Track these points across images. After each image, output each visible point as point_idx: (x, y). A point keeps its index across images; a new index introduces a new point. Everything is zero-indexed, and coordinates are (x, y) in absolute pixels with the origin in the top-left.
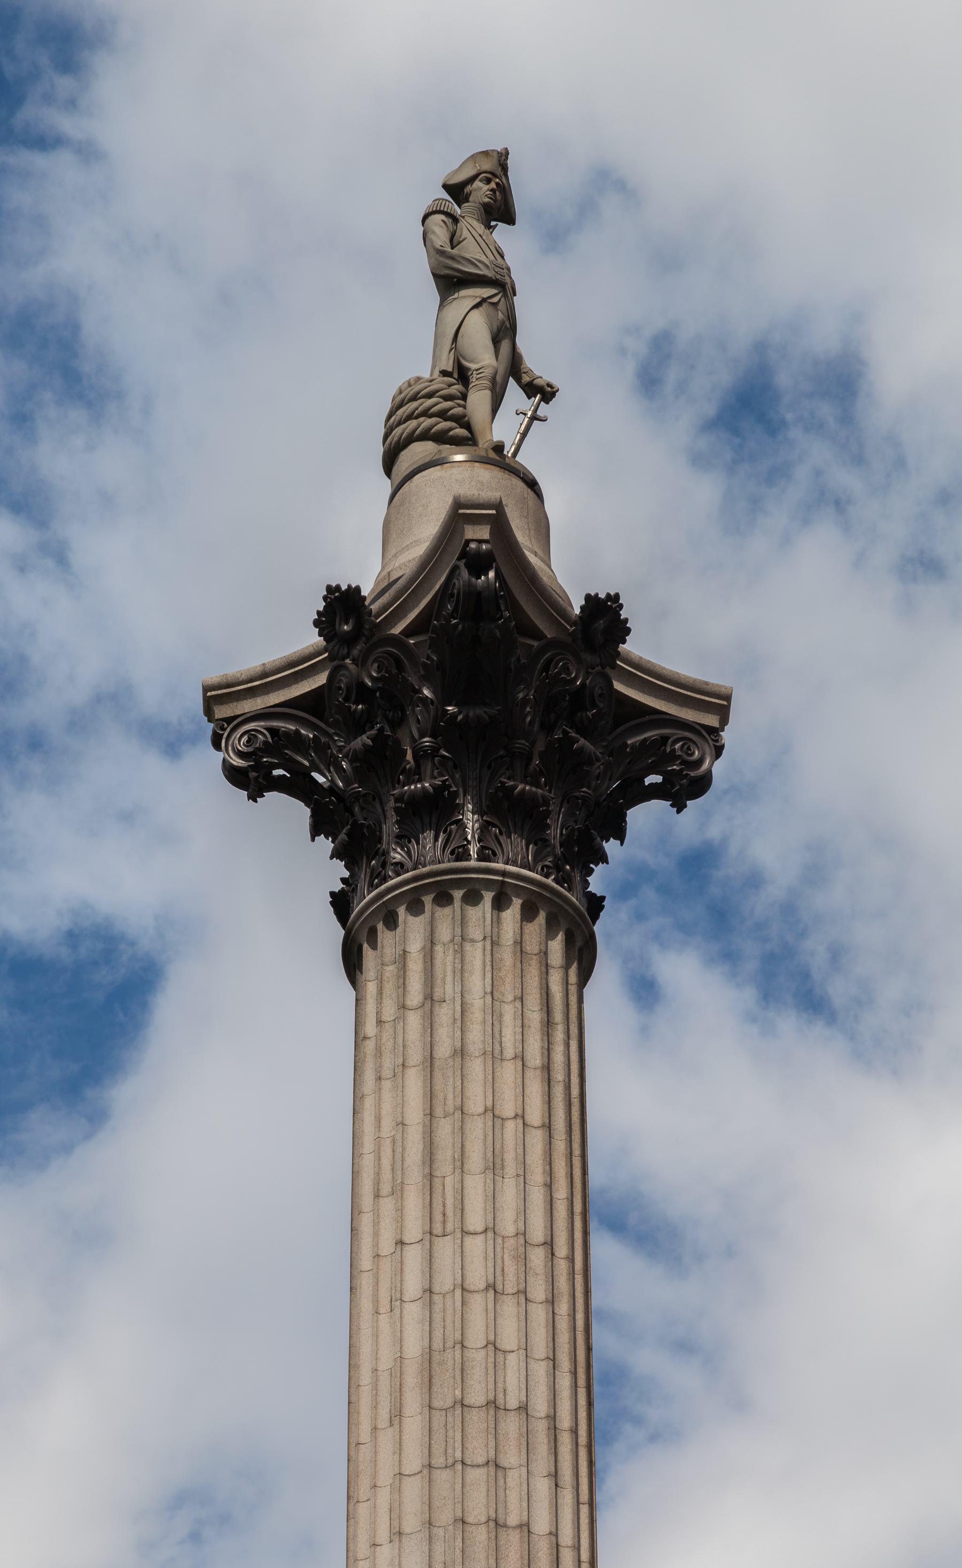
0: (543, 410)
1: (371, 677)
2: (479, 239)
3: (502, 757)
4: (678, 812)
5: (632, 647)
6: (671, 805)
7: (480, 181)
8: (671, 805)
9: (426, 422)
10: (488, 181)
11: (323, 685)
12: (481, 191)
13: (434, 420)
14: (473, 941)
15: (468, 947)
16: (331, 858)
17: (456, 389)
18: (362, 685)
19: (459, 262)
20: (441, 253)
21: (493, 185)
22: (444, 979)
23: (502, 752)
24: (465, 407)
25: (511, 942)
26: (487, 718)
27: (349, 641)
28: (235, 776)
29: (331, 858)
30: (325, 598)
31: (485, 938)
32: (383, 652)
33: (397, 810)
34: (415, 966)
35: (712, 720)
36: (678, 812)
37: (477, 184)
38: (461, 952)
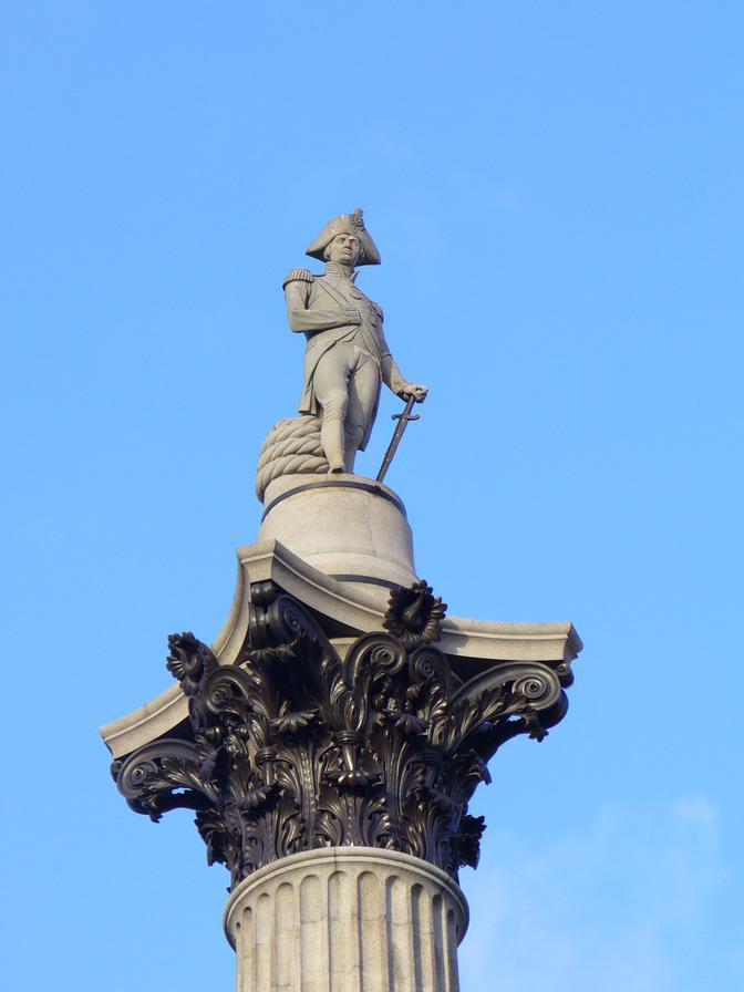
0: (417, 409)
1: (212, 703)
2: (333, 292)
3: (333, 748)
4: (540, 740)
5: (450, 616)
6: (530, 737)
7: (337, 242)
8: (530, 737)
9: (296, 460)
10: (343, 239)
11: (186, 720)
12: (337, 251)
13: (302, 457)
14: (313, 922)
15: (309, 928)
16: (211, 863)
17: (312, 425)
18: (208, 712)
19: (311, 318)
20: (296, 314)
21: (347, 243)
22: (289, 966)
23: (332, 744)
24: (319, 438)
25: (349, 916)
26: (305, 723)
27: (196, 676)
28: (137, 806)
29: (211, 863)
30: (170, 647)
31: (322, 918)
32: (222, 681)
33: (244, 816)
34: (265, 956)
35: (556, 653)
36: (540, 740)
37: (334, 244)
38: (300, 935)
